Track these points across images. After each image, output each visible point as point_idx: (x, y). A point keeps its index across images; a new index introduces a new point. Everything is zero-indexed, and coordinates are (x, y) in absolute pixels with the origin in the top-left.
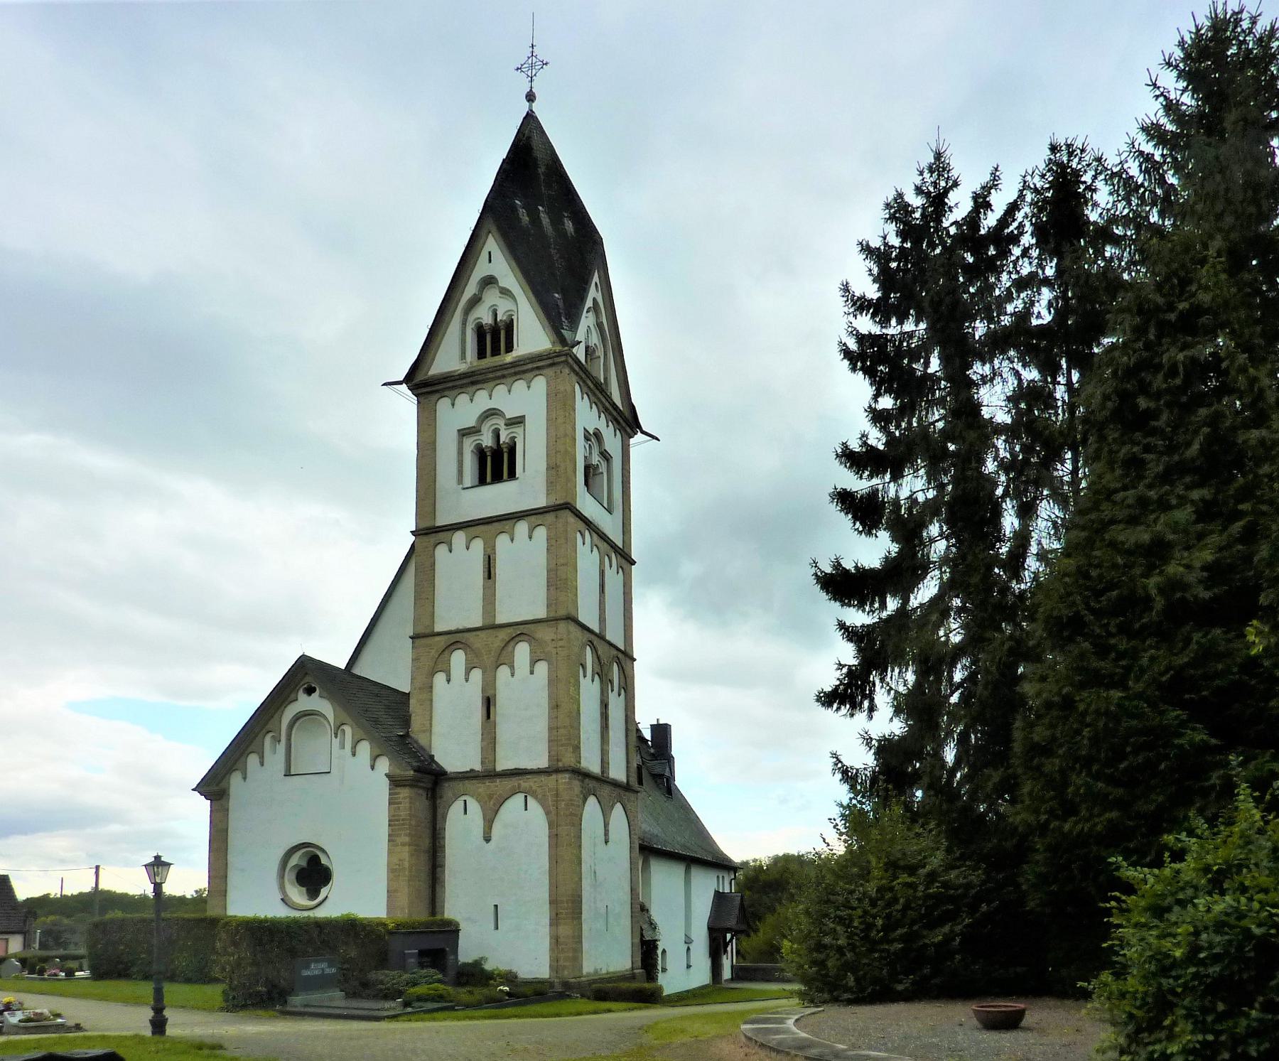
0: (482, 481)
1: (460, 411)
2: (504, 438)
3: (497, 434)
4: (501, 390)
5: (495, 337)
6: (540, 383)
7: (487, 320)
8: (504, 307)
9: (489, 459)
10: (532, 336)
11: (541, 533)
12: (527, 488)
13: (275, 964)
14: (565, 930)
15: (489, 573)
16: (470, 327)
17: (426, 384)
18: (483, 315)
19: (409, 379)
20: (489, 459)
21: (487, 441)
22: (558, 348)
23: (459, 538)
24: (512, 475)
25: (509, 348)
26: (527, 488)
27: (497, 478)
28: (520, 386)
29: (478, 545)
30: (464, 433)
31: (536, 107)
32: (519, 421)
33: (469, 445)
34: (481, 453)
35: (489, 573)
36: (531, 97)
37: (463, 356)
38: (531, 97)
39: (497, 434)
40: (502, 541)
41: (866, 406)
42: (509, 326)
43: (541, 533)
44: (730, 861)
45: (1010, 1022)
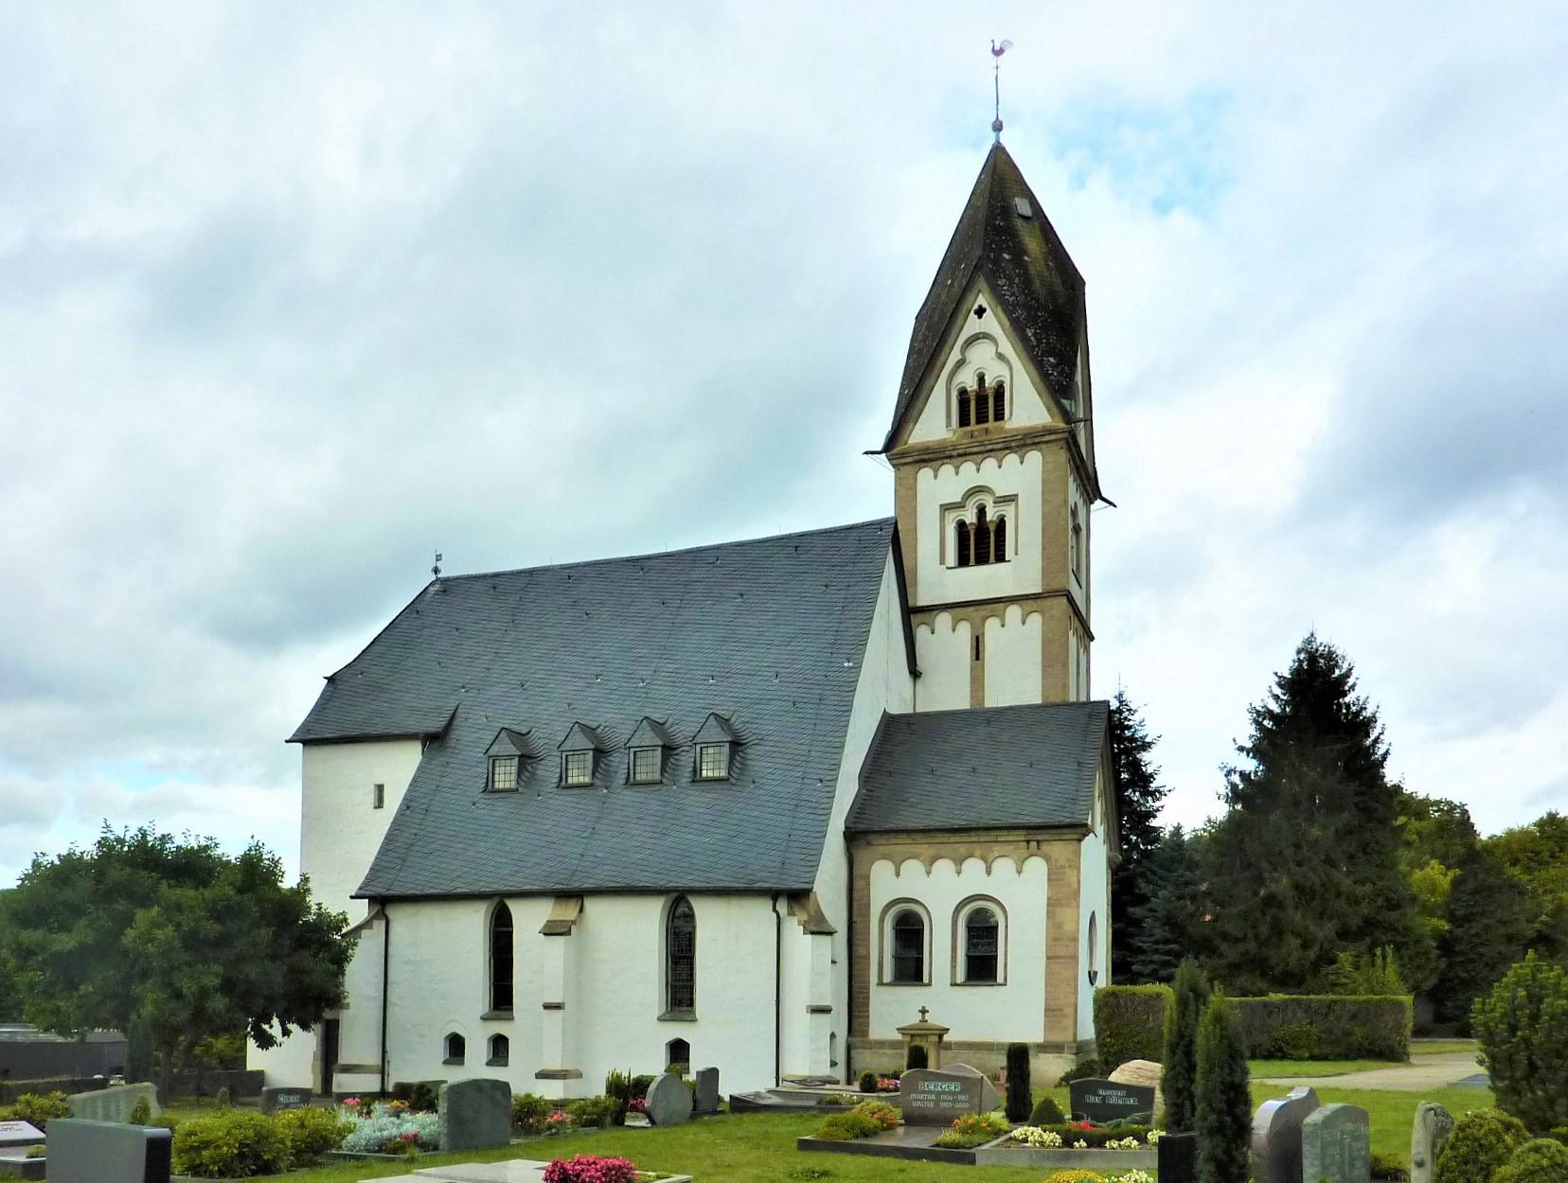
0: (963, 561)
1: (942, 486)
2: (991, 515)
3: (982, 511)
4: (990, 463)
5: (981, 406)
6: (1034, 457)
7: (972, 385)
8: (994, 373)
9: (973, 404)
11: (1035, 620)
12: (1021, 569)
13: (575, 895)
14: (683, 967)
15: (978, 652)
16: (954, 395)
17: (903, 455)
18: (968, 379)
19: (889, 446)
20: (973, 404)
21: (970, 517)
22: (1062, 425)
23: (944, 620)
24: (1001, 558)
25: (999, 416)
26: (1021, 569)
27: (982, 560)
28: (1012, 459)
29: (965, 631)
30: (946, 508)
31: (1007, 139)
32: (1011, 499)
34: (961, 525)
35: (978, 652)
36: (998, 127)
37: (949, 424)
38: (998, 127)
39: (982, 511)
40: (992, 625)
42: (999, 392)
43: (1035, 620)
44: (9, 891)
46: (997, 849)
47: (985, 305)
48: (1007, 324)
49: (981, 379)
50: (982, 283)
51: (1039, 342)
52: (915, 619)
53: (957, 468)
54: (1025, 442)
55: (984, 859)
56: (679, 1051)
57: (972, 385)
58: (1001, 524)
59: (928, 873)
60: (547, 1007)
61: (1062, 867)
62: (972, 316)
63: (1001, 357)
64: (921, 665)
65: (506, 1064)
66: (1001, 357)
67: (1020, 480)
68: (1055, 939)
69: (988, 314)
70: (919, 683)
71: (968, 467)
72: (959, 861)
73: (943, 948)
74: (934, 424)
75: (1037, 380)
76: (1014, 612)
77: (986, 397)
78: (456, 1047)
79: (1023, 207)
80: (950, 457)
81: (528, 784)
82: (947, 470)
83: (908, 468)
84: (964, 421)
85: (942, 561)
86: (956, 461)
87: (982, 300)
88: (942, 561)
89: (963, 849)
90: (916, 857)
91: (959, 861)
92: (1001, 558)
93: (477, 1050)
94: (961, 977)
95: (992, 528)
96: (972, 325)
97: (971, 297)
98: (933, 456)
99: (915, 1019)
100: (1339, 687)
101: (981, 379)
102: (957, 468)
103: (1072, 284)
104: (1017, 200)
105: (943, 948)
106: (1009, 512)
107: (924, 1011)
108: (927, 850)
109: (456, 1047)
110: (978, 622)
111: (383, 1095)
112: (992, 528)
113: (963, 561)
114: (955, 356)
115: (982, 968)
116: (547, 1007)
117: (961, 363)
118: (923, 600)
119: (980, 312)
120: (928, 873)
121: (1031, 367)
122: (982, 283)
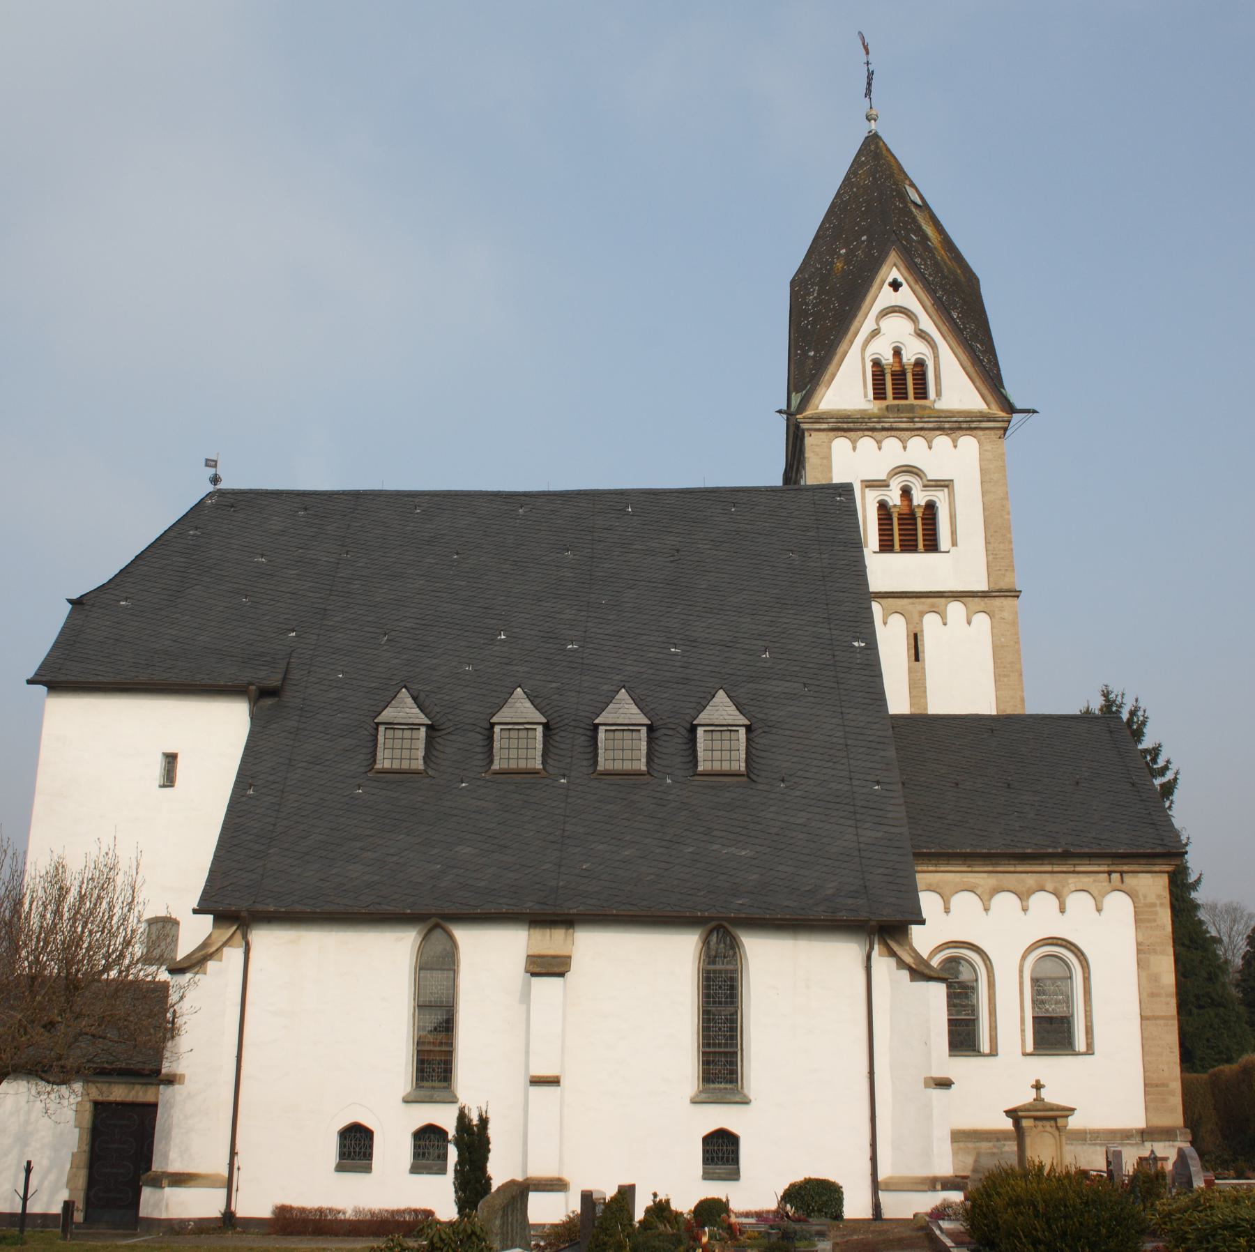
2: (920, 498)
3: (906, 493)
7: (887, 358)
8: (914, 350)
9: (889, 379)
16: (869, 365)
20: (889, 379)
21: (894, 497)
24: (932, 546)
25: (922, 393)
27: (909, 546)
28: (942, 441)
32: (945, 484)
34: (883, 506)
39: (906, 493)
46: (1073, 881)
47: (900, 279)
48: (928, 304)
49: (897, 353)
54: (956, 424)
55: (1057, 894)
56: (721, 1151)
57: (887, 358)
58: (931, 507)
59: (986, 910)
60: (554, 1081)
61: (1153, 905)
62: (887, 289)
65: (368, 1169)
66: (921, 334)
68: (1152, 995)
69: (905, 288)
72: (1023, 896)
73: (1008, 1012)
75: (968, 364)
78: (356, 1145)
80: (873, 430)
83: (823, 435)
84: (879, 394)
87: (895, 274)
89: (1031, 880)
90: (1042, 889)
91: (1023, 896)
92: (932, 546)
93: (394, 1148)
94: (1030, 1047)
95: (919, 513)
96: (885, 297)
99: (1028, 1097)
100: (1135, 730)
101: (897, 353)
102: (854, 442)
105: (1008, 1012)
106: (940, 498)
107: (1038, 1086)
108: (983, 879)
109: (356, 1145)
111: (505, 1215)
112: (919, 513)
115: (1053, 1033)
116: (554, 1081)
117: (875, 333)
119: (896, 285)
120: (986, 910)
121: (959, 351)
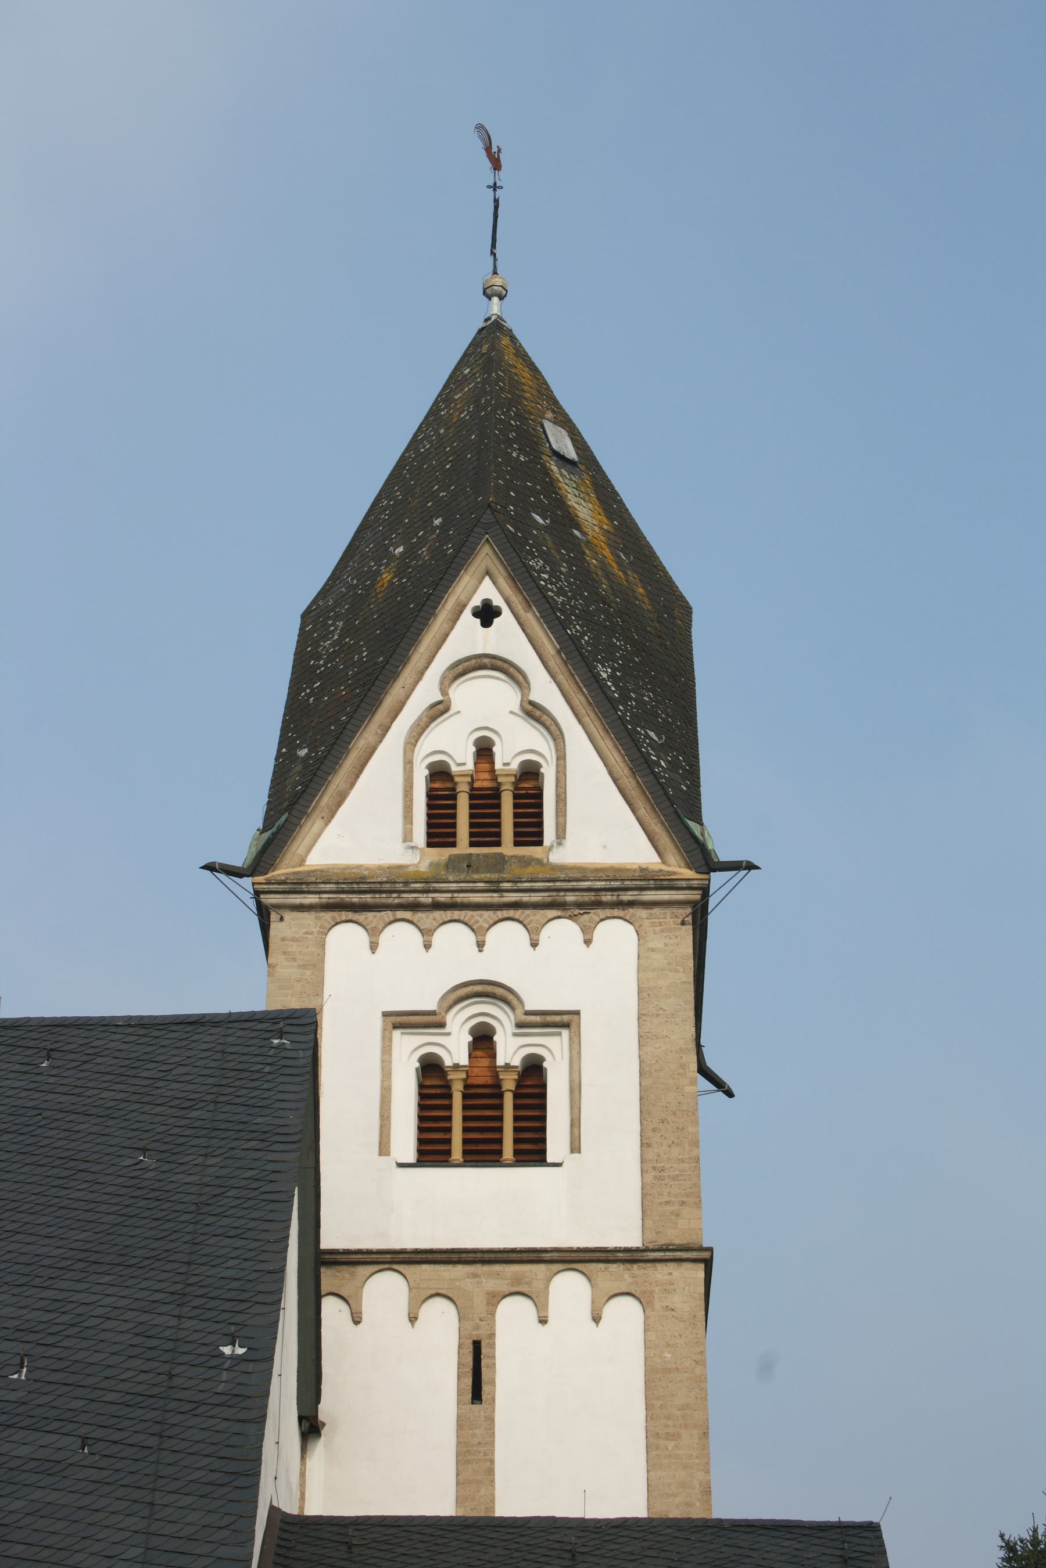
0: (432, 1151)
2: (510, 1050)
3: (483, 1040)
6: (617, 935)
7: (462, 759)
8: (517, 744)
10: (598, 823)
15: (476, 1384)
16: (421, 775)
18: (453, 744)
23: (385, 1290)
25: (530, 831)
26: (588, 1185)
27: (482, 1152)
28: (561, 931)
29: (442, 1321)
30: (402, 1021)
32: (561, 1021)
33: (409, 1049)
34: (430, 1068)
35: (476, 1384)
37: (407, 836)
39: (483, 1040)
40: (513, 1316)
41: (561, 848)
45: (486, 320)
47: (498, 601)
49: (484, 751)
50: (485, 556)
51: (625, 698)
52: (329, 1278)
53: (427, 934)
57: (462, 759)
58: (533, 1070)
62: (468, 621)
63: (534, 712)
64: (326, 1410)
66: (534, 712)
67: (587, 975)
69: (505, 621)
70: (319, 1449)
71: (454, 936)
74: (369, 823)
76: (569, 1289)
77: (495, 794)
79: (560, 441)
80: (415, 907)
81: (560, 844)
82: (401, 935)
84: (440, 832)
85: (384, 1149)
86: (426, 918)
87: (487, 591)
88: (384, 1149)
92: (532, 1151)
95: (509, 1083)
96: (466, 637)
97: (465, 581)
98: (365, 897)
101: (484, 751)
102: (427, 934)
103: (672, 613)
104: (548, 426)
106: (554, 1051)
110: (480, 1301)
112: (509, 1083)
113: (432, 1151)
114: (425, 693)
117: (439, 710)
118: (329, 1240)
119: (487, 614)
121: (608, 745)
122: (485, 556)
